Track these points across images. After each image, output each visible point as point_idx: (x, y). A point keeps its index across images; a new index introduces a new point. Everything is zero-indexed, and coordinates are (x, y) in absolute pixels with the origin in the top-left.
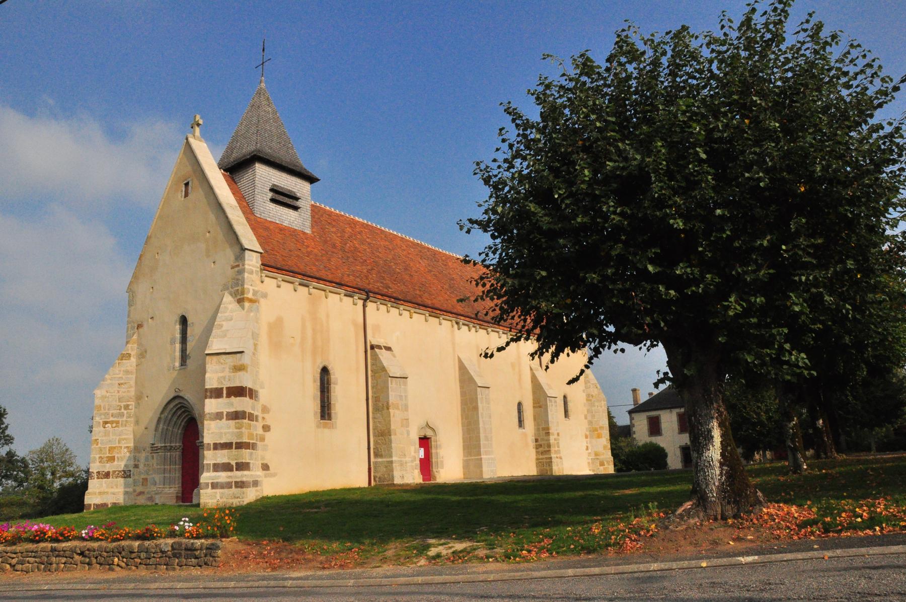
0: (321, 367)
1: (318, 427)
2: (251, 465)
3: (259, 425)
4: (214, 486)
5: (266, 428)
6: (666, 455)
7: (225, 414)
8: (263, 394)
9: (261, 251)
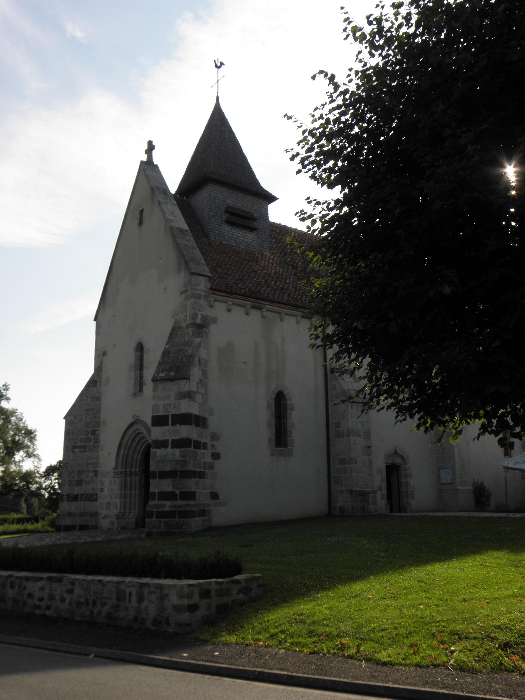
0: (276, 392)
1: (272, 455)
2: (197, 495)
3: (208, 452)
4: (161, 515)
5: (216, 456)
6: (353, 27)
7: (170, 441)
8: (213, 422)
9: (210, 275)
